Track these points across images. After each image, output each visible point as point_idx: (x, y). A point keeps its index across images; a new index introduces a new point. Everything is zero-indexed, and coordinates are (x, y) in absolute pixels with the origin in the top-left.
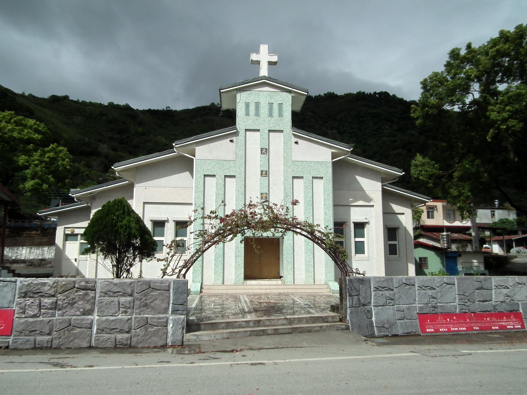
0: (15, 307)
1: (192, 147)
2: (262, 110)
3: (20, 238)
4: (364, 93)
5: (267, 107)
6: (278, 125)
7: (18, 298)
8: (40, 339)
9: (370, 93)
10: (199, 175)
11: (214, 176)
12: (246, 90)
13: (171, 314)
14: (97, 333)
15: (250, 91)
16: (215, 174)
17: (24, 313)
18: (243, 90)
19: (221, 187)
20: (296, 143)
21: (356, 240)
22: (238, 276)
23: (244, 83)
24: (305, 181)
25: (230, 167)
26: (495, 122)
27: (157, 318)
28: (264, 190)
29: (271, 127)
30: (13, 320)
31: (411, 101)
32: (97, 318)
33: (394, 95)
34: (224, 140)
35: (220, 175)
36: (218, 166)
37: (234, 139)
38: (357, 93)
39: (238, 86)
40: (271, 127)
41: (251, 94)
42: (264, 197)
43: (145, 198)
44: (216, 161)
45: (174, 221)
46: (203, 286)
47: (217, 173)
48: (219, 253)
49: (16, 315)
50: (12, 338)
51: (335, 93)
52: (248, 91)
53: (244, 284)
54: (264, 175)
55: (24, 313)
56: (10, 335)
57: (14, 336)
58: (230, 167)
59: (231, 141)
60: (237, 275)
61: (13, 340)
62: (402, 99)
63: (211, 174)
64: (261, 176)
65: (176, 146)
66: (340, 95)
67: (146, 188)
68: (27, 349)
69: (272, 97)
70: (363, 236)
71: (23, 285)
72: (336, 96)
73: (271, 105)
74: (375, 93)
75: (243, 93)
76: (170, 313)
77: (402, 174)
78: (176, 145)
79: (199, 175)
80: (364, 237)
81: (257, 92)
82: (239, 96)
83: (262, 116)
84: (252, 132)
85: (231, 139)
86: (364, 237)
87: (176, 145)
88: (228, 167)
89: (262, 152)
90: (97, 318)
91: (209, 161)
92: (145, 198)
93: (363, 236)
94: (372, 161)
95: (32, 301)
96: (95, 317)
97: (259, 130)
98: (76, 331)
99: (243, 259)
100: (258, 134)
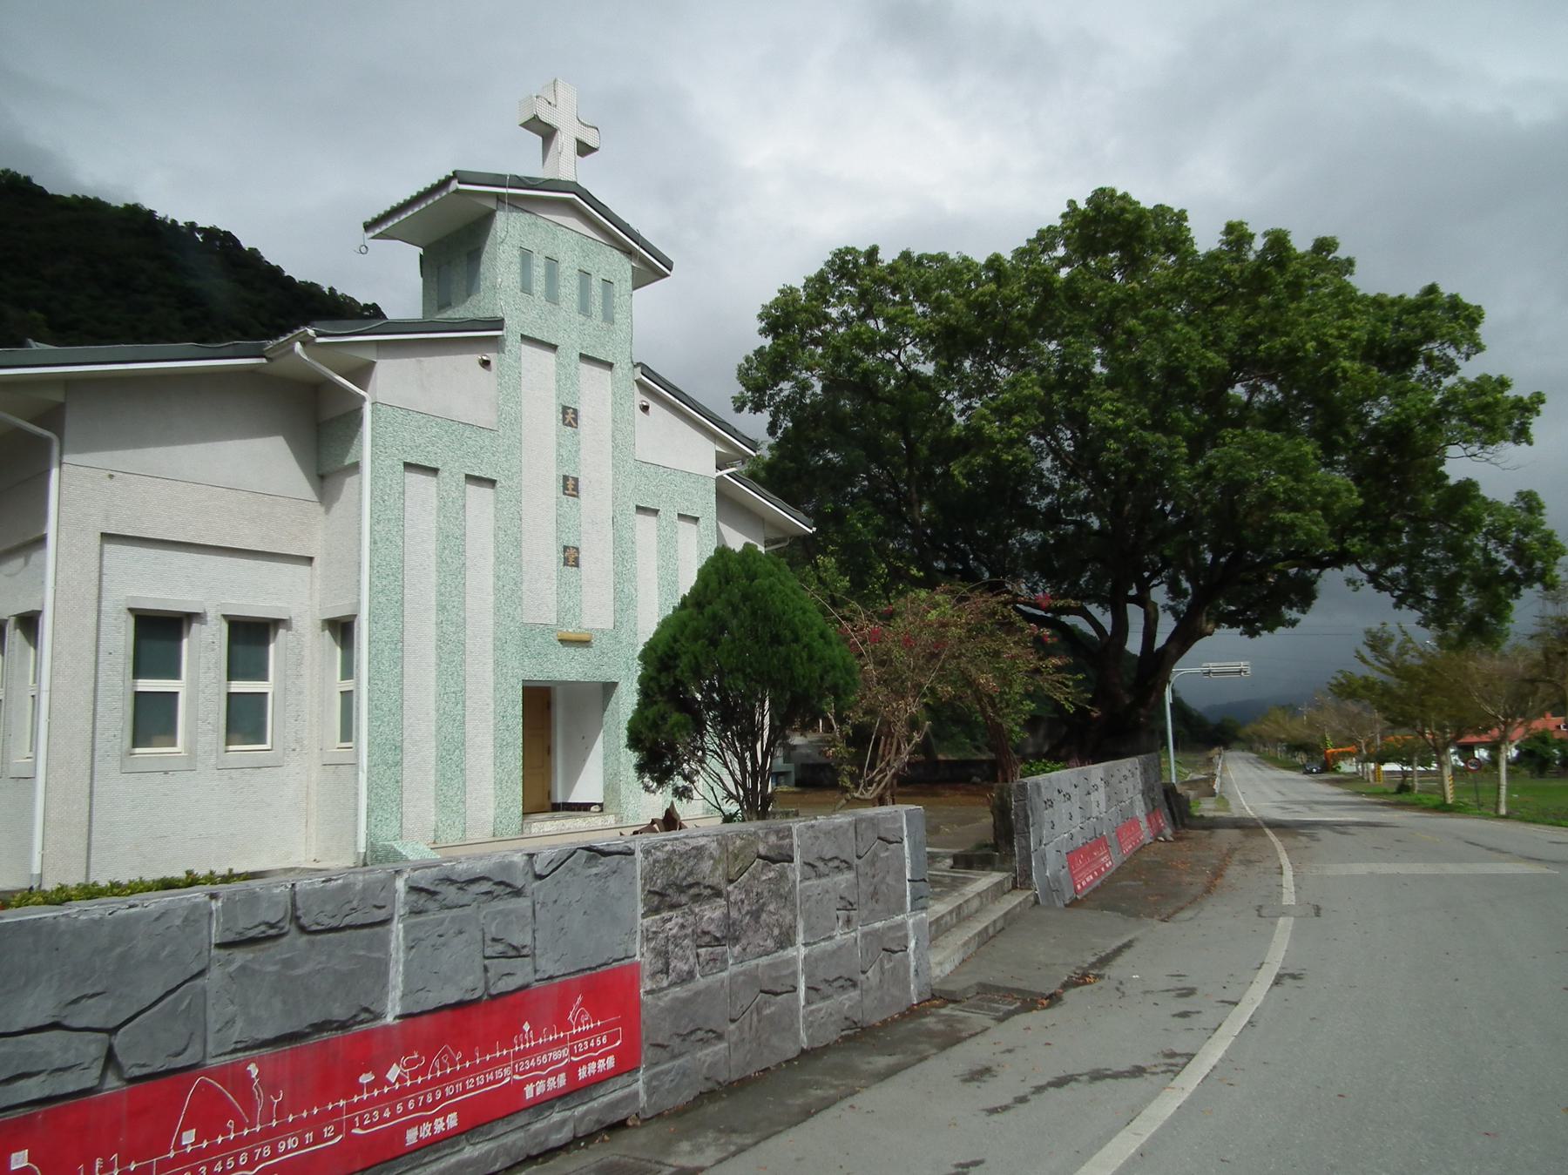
0: (641, 954)
1: (367, 355)
2: (565, 286)
3: (636, 678)
4: (151, 213)
5: (575, 282)
6: (603, 346)
7: (644, 916)
8: (709, 1060)
9: (174, 222)
10: (388, 462)
11: (435, 471)
12: (525, 208)
13: (912, 910)
14: (808, 1002)
15: (533, 216)
16: (439, 466)
17: (666, 971)
18: (516, 207)
19: (458, 514)
20: (645, 409)
21: (232, 690)
22: (507, 810)
23: (523, 186)
24: (664, 523)
25: (481, 448)
26: (992, 442)
27: (1118, 911)
28: (572, 539)
29: (585, 344)
30: (638, 1003)
31: (306, 283)
32: (803, 951)
33: (254, 252)
34: (461, 354)
35: (453, 471)
36: (446, 439)
37: (491, 356)
38: (127, 207)
39: (510, 187)
40: (585, 344)
41: (535, 224)
42: (571, 559)
43: (107, 518)
44: (439, 420)
45: (225, 616)
46: (1494, 806)
47: (444, 464)
48: (453, 738)
49: (647, 984)
50: (641, 1075)
51: (36, 181)
52: (528, 215)
53: (523, 833)
54: (570, 492)
55: (666, 971)
56: (637, 1069)
57: (647, 1069)
58: (481, 448)
59: (486, 364)
60: (504, 805)
61: (648, 1084)
62: (277, 271)
63: (426, 464)
64: (565, 494)
65: (320, 340)
66: (56, 193)
67: (111, 476)
68: (441, 1141)
69: (588, 255)
70: (261, 674)
71: (656, 861)
72: (40, 192)
73: (585, 275)
74: (192, 226)
75: (514, 214)
76: (909, 909)
77: (811, 531)
78: (318, 336)
79: (388, 462)
80: (264, 678)
81: (550, 224)
82: (504, 219)
83: (563, 305)
84: (536, 350)
85: (485, 358)
86: (264, 678)
87: (320, 335)
88: (474, 449)
89: (564, 419)
90: (803, 951)
91: (419, 417)
92: (107, 518)
93: (261, 674)
94: (763, 490)
95: (680, 920)
96: (799, 952)
97: (553, 348)
98: (773, 1009)
99: (519, 752)
100: (549, 356)
